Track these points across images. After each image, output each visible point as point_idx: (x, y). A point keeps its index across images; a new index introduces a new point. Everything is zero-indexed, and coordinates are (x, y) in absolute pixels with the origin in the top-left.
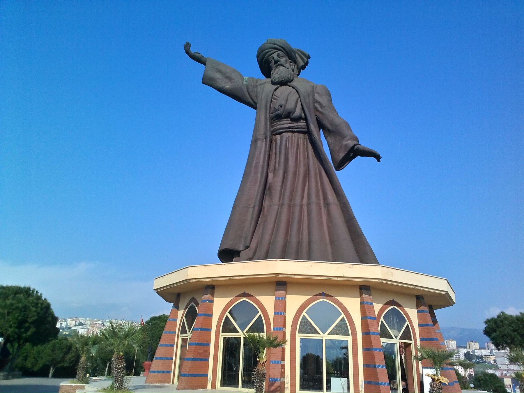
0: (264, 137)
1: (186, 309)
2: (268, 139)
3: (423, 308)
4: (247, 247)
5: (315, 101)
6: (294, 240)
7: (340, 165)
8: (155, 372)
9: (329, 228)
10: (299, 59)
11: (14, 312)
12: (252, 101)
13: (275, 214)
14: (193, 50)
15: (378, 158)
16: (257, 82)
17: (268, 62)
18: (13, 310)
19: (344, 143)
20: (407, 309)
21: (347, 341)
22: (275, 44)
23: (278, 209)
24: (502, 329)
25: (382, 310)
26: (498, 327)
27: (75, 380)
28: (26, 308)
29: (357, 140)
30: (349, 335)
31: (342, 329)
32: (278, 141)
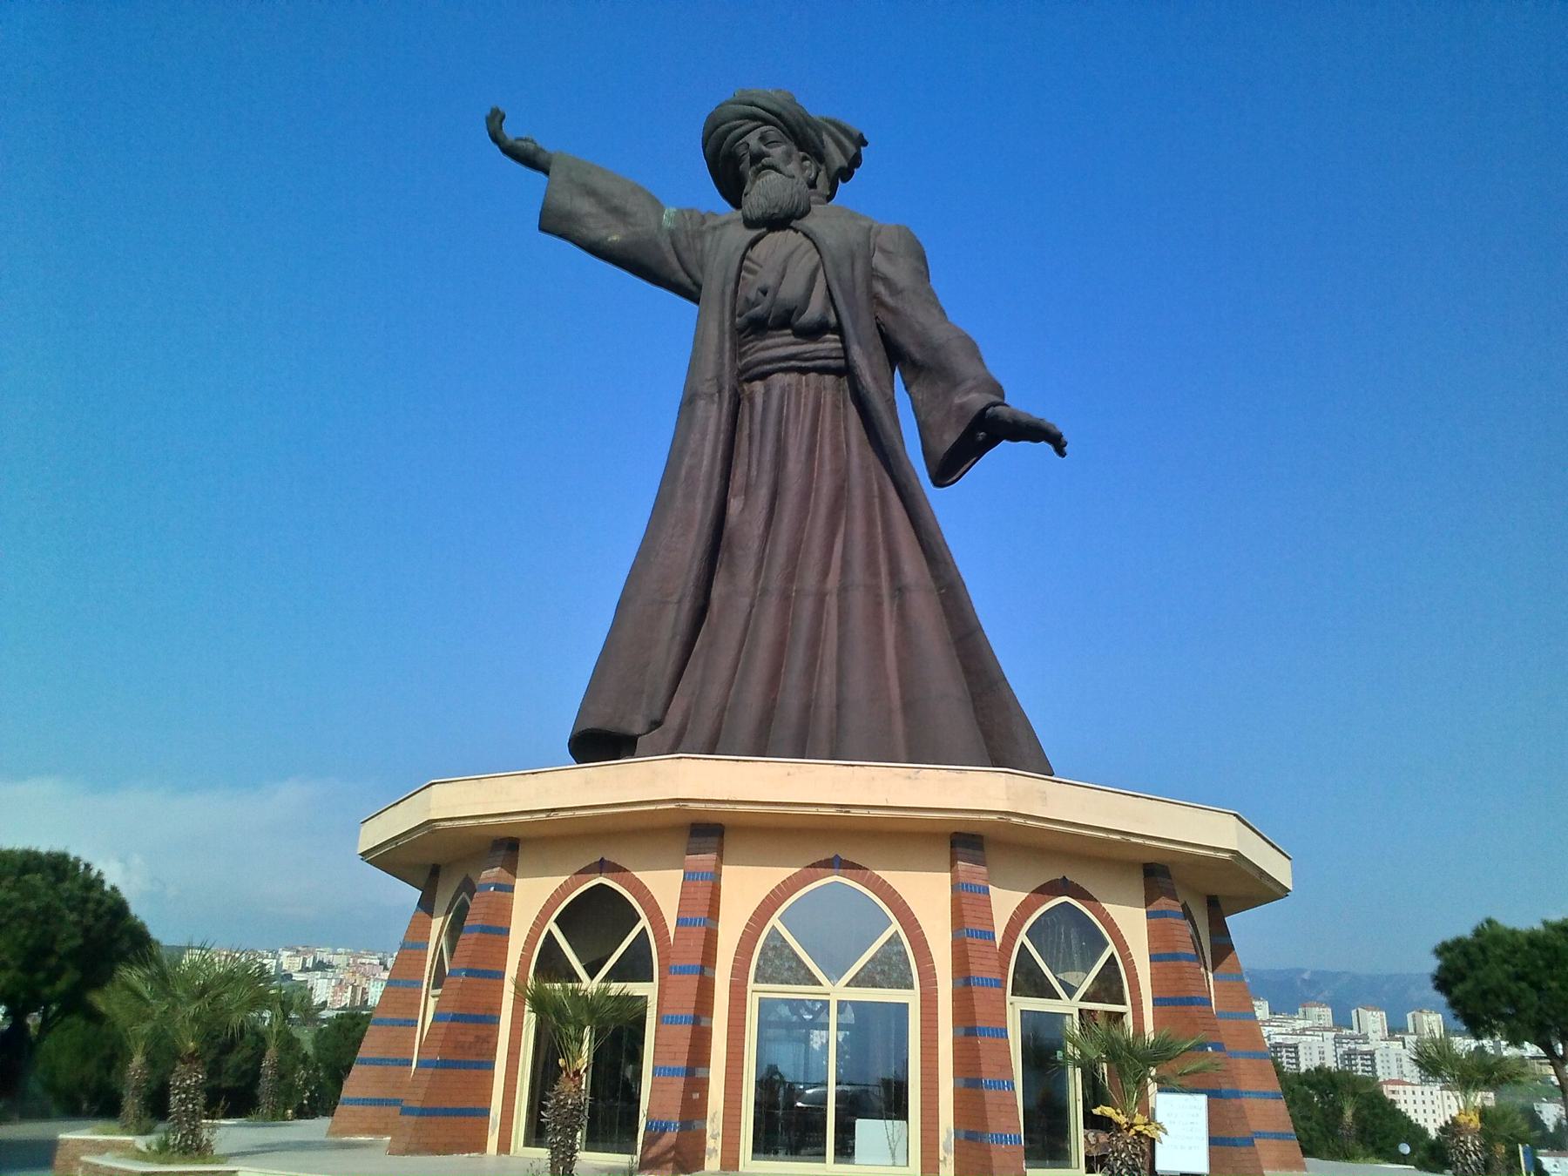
0: (714, 390)
1: (448, 913)
2: (726, 394)
3: (1163, 903)
4: (656, 724)
5: (873, 274)
6: (791, 701)
7: (946, 470)
8: (357, 1102)
9: (902, 662)
10: (831, 148)
11: (15, 925)
12: (687, 281)
13: (741, 622)
14: (510, 132)
15: (1058, 444)
16: (703, 221)
17: (733, 159)
18: (13, 918)
19: (957, 401)
20: (1110, 908)
21: (906, 1005)
22: (752, 104)
23: (752, 606)
24: (1480, 974)
25: (1024, 910)
26: (1471, 965)
27: (114, 1125)
28: (48, 914)
29: (998, 390)
30: (911, 987)
31: (888, 970)
32: (759, 400)
